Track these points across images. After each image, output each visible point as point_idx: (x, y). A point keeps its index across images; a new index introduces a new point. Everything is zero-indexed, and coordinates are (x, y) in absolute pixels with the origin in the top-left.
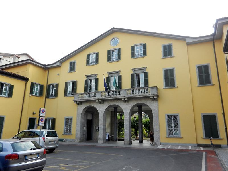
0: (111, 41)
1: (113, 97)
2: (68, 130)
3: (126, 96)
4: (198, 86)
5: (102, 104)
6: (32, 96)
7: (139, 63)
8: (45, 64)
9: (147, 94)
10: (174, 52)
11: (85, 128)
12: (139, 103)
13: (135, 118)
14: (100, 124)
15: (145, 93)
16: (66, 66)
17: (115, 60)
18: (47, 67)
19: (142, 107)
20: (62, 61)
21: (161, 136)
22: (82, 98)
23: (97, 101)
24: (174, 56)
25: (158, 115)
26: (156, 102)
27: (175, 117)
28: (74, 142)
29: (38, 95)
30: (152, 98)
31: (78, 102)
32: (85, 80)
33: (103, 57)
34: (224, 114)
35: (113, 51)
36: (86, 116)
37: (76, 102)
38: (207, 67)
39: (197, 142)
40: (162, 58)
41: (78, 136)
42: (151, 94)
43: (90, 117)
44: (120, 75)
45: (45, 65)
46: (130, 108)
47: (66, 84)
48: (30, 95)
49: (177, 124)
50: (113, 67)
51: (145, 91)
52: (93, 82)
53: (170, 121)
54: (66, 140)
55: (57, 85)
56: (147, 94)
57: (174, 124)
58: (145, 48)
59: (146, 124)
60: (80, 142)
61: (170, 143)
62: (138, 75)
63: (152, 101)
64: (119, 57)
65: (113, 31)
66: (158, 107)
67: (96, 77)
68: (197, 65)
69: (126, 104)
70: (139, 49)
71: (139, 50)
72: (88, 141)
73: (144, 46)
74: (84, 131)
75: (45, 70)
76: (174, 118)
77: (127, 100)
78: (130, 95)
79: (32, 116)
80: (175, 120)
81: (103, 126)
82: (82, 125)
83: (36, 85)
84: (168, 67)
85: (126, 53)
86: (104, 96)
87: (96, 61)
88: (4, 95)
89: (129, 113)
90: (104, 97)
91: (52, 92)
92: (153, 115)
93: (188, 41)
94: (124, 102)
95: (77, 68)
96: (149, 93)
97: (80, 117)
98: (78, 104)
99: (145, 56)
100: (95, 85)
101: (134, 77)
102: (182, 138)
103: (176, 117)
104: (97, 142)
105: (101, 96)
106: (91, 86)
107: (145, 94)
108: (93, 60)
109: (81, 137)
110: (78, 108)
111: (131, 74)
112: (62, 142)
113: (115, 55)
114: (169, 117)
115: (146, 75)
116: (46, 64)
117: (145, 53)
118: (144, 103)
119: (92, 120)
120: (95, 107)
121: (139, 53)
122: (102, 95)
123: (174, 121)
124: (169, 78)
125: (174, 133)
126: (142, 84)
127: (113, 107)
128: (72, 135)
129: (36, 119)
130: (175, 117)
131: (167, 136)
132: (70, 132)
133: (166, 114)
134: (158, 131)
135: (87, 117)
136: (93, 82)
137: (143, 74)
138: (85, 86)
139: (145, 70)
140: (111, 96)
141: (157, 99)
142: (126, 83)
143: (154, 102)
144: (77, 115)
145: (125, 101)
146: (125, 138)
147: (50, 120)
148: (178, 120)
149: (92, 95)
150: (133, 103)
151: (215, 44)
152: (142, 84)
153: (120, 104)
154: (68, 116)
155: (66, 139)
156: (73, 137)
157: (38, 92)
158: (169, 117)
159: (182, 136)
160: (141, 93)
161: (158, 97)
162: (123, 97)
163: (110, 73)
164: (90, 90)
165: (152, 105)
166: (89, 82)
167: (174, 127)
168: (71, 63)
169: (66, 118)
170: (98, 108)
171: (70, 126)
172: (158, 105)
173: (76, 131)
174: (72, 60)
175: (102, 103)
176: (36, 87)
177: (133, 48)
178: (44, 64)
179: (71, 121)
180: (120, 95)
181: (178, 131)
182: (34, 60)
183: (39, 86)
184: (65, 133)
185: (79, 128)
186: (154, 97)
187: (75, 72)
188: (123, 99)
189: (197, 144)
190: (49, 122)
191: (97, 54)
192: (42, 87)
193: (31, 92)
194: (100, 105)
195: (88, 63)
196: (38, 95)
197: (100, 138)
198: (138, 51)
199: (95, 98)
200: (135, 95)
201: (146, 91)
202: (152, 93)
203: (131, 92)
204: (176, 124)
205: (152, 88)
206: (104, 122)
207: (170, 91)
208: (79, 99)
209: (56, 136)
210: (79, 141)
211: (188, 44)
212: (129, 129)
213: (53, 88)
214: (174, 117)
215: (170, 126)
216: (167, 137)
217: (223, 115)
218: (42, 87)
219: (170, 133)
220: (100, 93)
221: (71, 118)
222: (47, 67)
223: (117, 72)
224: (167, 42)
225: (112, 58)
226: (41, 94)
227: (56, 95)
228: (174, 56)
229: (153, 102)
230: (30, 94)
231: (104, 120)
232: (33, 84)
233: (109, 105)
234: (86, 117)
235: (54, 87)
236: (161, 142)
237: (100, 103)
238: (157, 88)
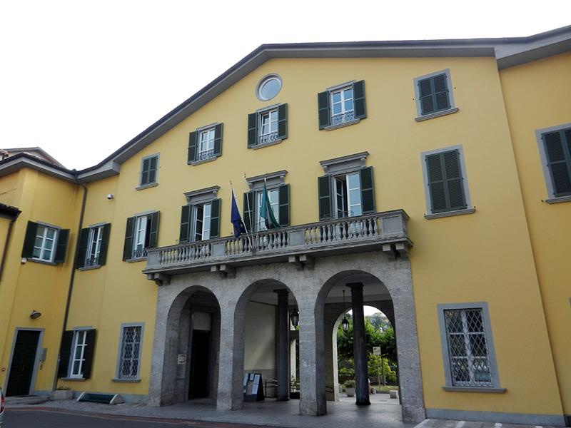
0: (259, 87)
1: (260, 256)
2: (129, 366)
3: (302, 247)
4: (550, 202)
5: (231, 277)
6: (31, 264)
7: (342, 143)
8: (75, 170)
9: (371, 237)
10: (457, 96)
11: (181, 359)
12: (348, 269)
13: (345, 325)
14: (222, 343)
16: (133, 170)
17: (344, 121)
18: (80, 177)
19: (364, 288)
20: (122, 156)
21: (425, 385)
23: (214, 269)
24: (457, 110)
25: (412, 309)
26: (404, 264)
27: (475, 316)
28: (146, 405)
29: (51, 261)
30: (387, 249)
31: (157, 276)
32: (183, 207)
33: (236, 134)
35: (265, 115)
36: (187, 319)
37: (153, 274)
38: (370, 171)
39: (564, 413)
40: (418, 120)
41: (158, 385)
42: (383, 236)
43: (201, 324)
44: (286, 183)
45: (74, 173)
46: (319, 288)
47: (131, 223)
48: (24, 260)
49: (483, 340)
50: (265, 162)
52: (207, 210)
53: (454, 331)
54: (122, 400)
55: (107, 228)
56: (371, 237)
57: (472, 341)
58: (362, 96)
59: (388, 344)
60: (162, 404)
61: (461, 411)
62: (342, 184)
63: (391, 260)
64: (283, 131)
65: (266, 55)
66: (412, 282)
67: (215, 195)
68: (462, 148)
69: (306, 277)
70: (343, 101)
71: (342, 104)
72: (193, 401)
73: (359, 88)
74: (179, 367)
75: (78, 190)
76: (469, 320)
77: (310, 261)
78: (315, 245)
79: (27, 325)
80: (473, 325)
81: (234, 350)
82: (172, 349)
83: (46, 231)
84: (440, 145)
85: (304, 116)
86: (237, 252)
87: (215, 147)
89: (314, 305)
90: (233, 256)
91: (93, 252)
92: (395, 311)
93: (502, 52)
94: (299, 270)
96: (375, 234)
97: (164, 324)
98: (160, 282)
99: (361, 119)
100: (212, 220)
101: (332, 188)
102: (505, 391)
103: (477, 314)
104: (213, 405)
105: (226, 252)
106: (200, 225)
107: (365, 237)
108: (207, 147)
109: (167, 390)
110: (159, 297)
111: (320, 179)
112: (106, 406)
113: (271, 125)
114: (452, 318)
115: (367, 178)
116: (78, 169)
117: (360, 110)
118: (364, 270)
119: (209, 331)
120: (211, 289)
121: (343, 112)
122: (229, 249)
123: (470, 330)
124: (445, 180)
125: (471, 375)
126: (354, 205)
127: (274, 291)
128: (140, 381)
129: (41, 335)
130: (475, 316)
131: (447, 384)
132: (135, 373)
134: (413, 365)
135: (191, 322)
136: (207, 210)
137: (357, 177)
138: (182, 227)
139: (364, 162)
140: (254, 250)
141: (404, 252)
142: (305, 208)
143: (398, 266)
144: (157, 317)
145: (301, 266)
146: (303, 393)
147: (81, 333)
148: (483, 324)
149: (204, 249)
150: (326, 272)
152: (354, 205)
153: (286, 278)
154: (132, 321)
155: (119, 396)
156: (142, 389)
157: (53, 250)
158: (452, 318)
159: (502, 386)
160: (357, 234)
161: (409, 245)
162: (294, 251)
163: (254, 182)
164: (199, 237)
165: (391, 277)
166: (195, 212)
167: (473, 352)
168: (146, 162)
169: (125, 328)
170: (217, 294)
171: (137, 353)
172: (410, 275)
173: (152, 368)
174: (148, 153)
175: (231, 274)
176: (45, 237)
177: (323, 99)
178: (70, 168)
179: (138, 338)
180: (327, 239)
181: (485, 364)
182: (55, 161)
183: (56, 233)
184: (120, 377)
185: (160, 361)
186: (393, 245)
187: (157, 185)
188: (292, 260)
189: (564, 415)
190: (80, 342)
191: (219, 129)
192: (64, 235)
193: (29, 251)
194: (226, 283)
195: (193, 156)
196: (51, 261)
197: (222, 393)
198: (338, 107)
199: (207, 259)
200: (329, 244)
201: (368, 228)
202: (390, 231)
203: (365, 229)
204: (478, 341)
205: (389, 215)
206: (235, 338)
207: (451, 225)
208: (163, 265)
209: (113, 396)
210: (158, 401)
211: (505, 66)
212: (314, 360)
213: (95, 239)
214: (471, 314)
215: (455, 347)
216: (447, 390)
218: (64, 235)
219: (459, 374)
220: (223, 245)
221: (139, 328)
222: (80, 177)
223: (279, 176)
224: (429, 69)
225: (260, 134)
226: (60, 257)
227: (102, 260)
228: (457, 110)
229: (392, 263)
230: (23, 256)
231: (235, 330)
232: (33, 229)
233: (250, 280)
234: (186, 324)
235: (98, 237)
236: (427, 407)
237: (225, 275)
238: (406, 218)
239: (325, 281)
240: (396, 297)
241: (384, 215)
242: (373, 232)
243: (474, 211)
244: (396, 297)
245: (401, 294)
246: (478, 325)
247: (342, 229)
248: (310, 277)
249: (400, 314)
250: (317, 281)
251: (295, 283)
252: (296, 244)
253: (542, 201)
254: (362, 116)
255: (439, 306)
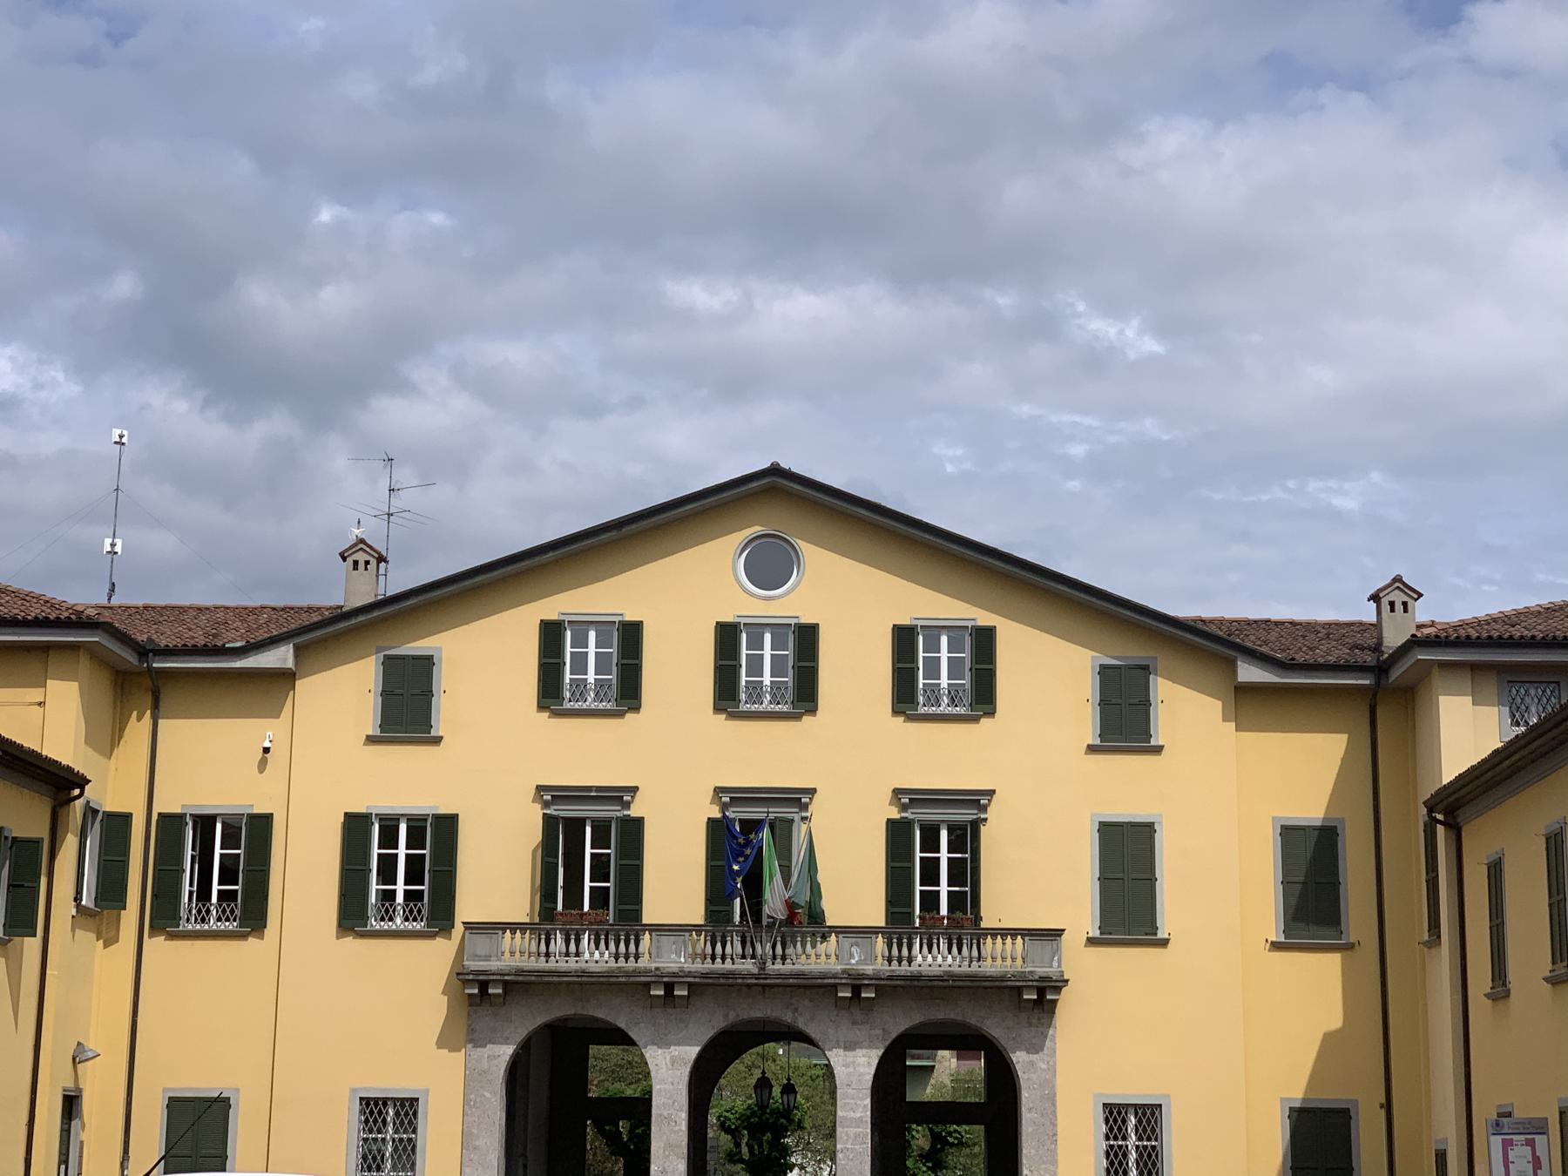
15: (713, 958)
22: (514, 953)
27: (1149, 1116)
32: (1290, 834)
34: (1388, 1106)
51: (895, 951)
68: (1280, 818)
88: (928, 703)
95: (447, 710)
111: (891, 823)
114: (1114, 1115)
130: (1149, 1116)
133: (1096, 1096)
143: (1034, 1021)
151: (1380, 711)
153: (812, 1019)
158: (1114, 1115)
217: (1383, 1113)
239: (894, 1035)
240: (1026, 1077)
241: (845, 932)
242: (723, 958)
243: (1164, 943)
244: (1026, 1077)
245: (1035, 1073)
246: (1153, 1130)
247: (774, 947)
248: (862, 1023)
249: (1031, 1105)
250: (879, 1032)
251: (831, 1031)
252: (820, 958)
253: (1267, 940)
254: (987, 708)
255: (1096, 1096)
